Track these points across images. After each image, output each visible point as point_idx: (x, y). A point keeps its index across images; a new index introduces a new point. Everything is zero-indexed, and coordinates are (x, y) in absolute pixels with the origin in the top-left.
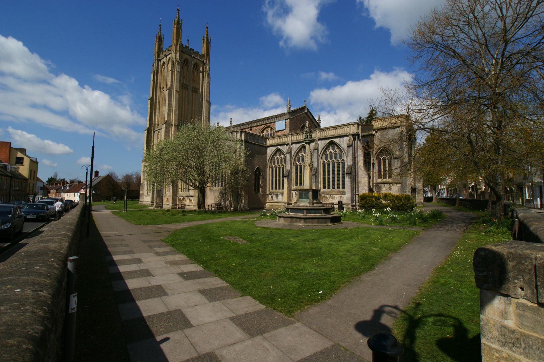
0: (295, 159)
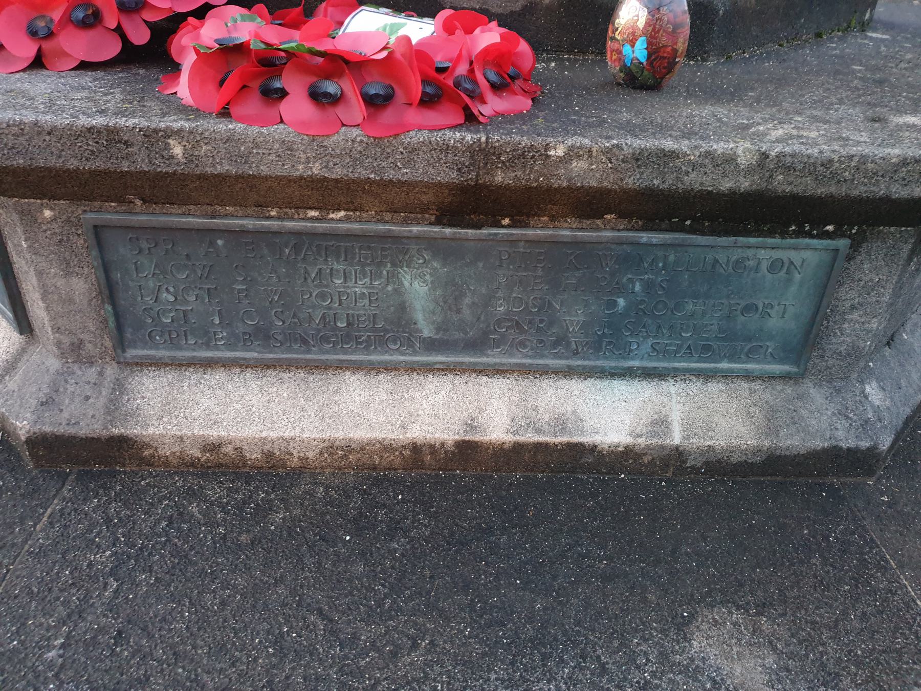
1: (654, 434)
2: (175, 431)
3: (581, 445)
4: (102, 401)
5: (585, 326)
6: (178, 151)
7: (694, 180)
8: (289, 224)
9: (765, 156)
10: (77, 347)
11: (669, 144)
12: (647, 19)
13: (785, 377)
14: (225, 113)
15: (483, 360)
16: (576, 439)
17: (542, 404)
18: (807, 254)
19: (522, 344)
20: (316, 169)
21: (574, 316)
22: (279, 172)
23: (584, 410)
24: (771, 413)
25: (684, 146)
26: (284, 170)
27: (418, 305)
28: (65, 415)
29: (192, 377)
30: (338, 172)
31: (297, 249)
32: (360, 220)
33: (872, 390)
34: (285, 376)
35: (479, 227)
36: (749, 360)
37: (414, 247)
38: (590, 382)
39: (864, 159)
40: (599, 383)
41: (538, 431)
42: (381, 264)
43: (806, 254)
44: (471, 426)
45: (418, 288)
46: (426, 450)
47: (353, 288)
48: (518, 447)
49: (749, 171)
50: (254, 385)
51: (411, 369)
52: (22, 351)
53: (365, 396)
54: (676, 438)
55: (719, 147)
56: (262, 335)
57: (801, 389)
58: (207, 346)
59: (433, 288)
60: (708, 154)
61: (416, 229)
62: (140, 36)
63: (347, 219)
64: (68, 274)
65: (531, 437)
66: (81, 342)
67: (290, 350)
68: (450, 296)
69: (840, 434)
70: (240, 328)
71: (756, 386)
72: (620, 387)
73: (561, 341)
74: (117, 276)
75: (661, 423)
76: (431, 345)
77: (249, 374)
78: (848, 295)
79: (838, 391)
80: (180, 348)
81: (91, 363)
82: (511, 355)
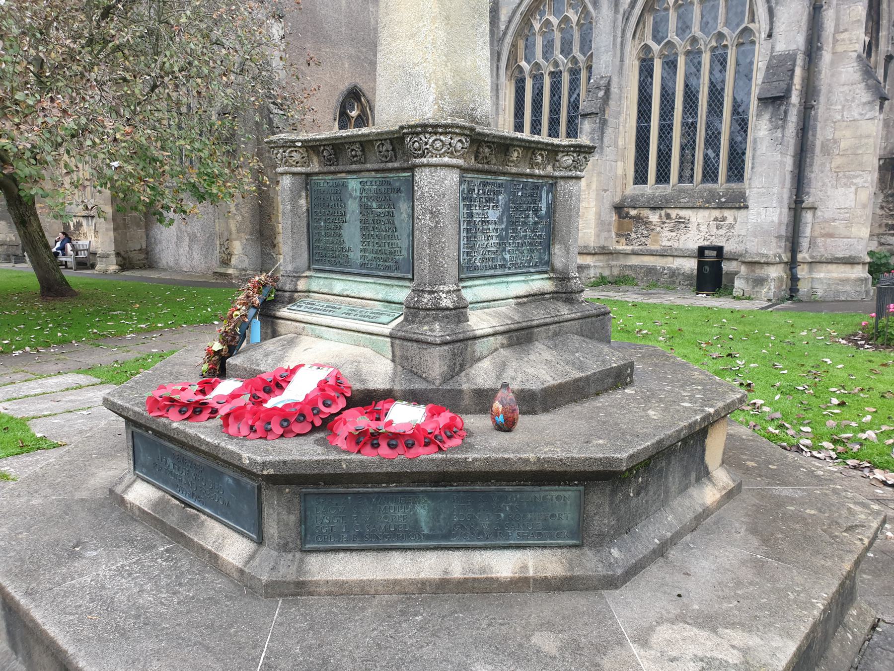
0: (514, 45)
1: (521, 572)
2: (325, 578)
3: (492, 578)
4: (295, 567)
5: (489, 526)
6: (344, 466)
7: (517, 468)
8: (376, 489)
9: (539, 458)
10: (286, 544)
11: (506, 456)
12: (435, 579)
13: (575, 546)
14: (359, 452)
15: (450, 543)
16: (489, 576)
17: (475, 562)
18: (570, 493)
19: (465, 535)
20: (390, 469)
21: (485, 522)
22: (377, 471)
23: (492, 563)
24: (570, 561)
25: (512, 456)
26: (379, 470)
27: (423, 519)
28: (281, 573)
29: (331, 556)
30: (397, 470)
31: (377, 499)
32: (401, 486)
33: (615, 552)
34: (368, 554)
35: (445, 486)
36: (558, 539)
37: (421, 496)
38: (495, 551)
39: (573, 458)
40: (499, 552)
41: (474, 573)
42: (409, 503)
43: (570, 493)
44: (446, 572)
45: (422, 512)
46: (428, 584)
47: (397, 514)
48: (466, 580)
49: (535, 463)
50: (356, 558)
51: (420, 549)
52: (256, 551)
53: (401, 561)
54: (531, 573)
55: (523, 456)
56: (361, 536)
57: (583, 551)
58: (339, 542)
59: (428, 512)
60: (520, 458)
61: (422, 489)
62: (318, 423)
63: (396, 486)
64: (289, 513)
65: (471, 576)
66: (288, 542)
67: (371, 542)
68: (435, 515)
69: (600, 569)
70: (353, 533)
71: (564, 550)
72: (507, 553)
73: (481, 533)
74: (308, 513)
75: (525, 568)
76: (429, 538)
77: (354, 554)
78: (591, 509)
79: (599, 551)
80: (327, 543)
81: (290, 552)
82: (461, 541)
